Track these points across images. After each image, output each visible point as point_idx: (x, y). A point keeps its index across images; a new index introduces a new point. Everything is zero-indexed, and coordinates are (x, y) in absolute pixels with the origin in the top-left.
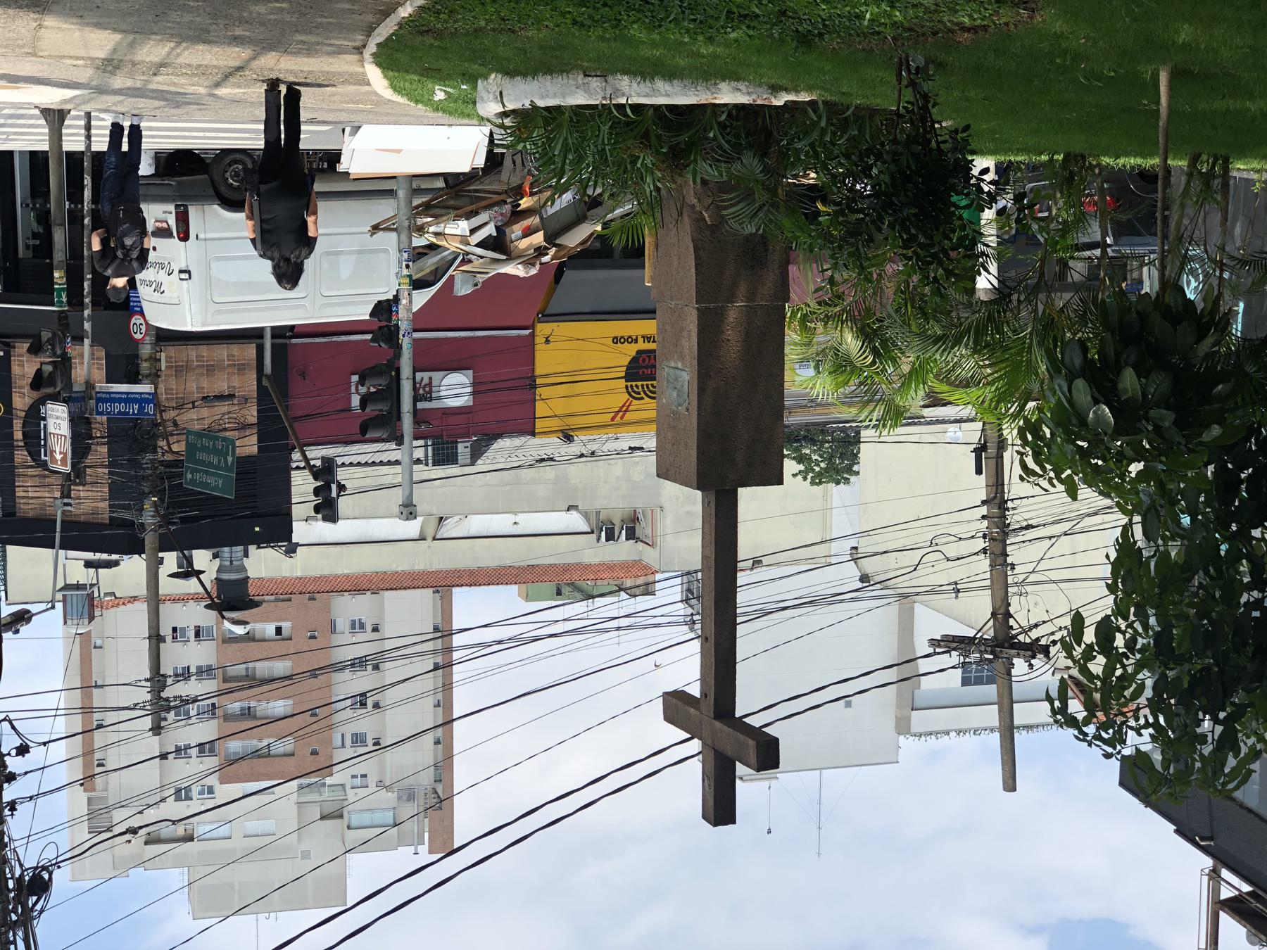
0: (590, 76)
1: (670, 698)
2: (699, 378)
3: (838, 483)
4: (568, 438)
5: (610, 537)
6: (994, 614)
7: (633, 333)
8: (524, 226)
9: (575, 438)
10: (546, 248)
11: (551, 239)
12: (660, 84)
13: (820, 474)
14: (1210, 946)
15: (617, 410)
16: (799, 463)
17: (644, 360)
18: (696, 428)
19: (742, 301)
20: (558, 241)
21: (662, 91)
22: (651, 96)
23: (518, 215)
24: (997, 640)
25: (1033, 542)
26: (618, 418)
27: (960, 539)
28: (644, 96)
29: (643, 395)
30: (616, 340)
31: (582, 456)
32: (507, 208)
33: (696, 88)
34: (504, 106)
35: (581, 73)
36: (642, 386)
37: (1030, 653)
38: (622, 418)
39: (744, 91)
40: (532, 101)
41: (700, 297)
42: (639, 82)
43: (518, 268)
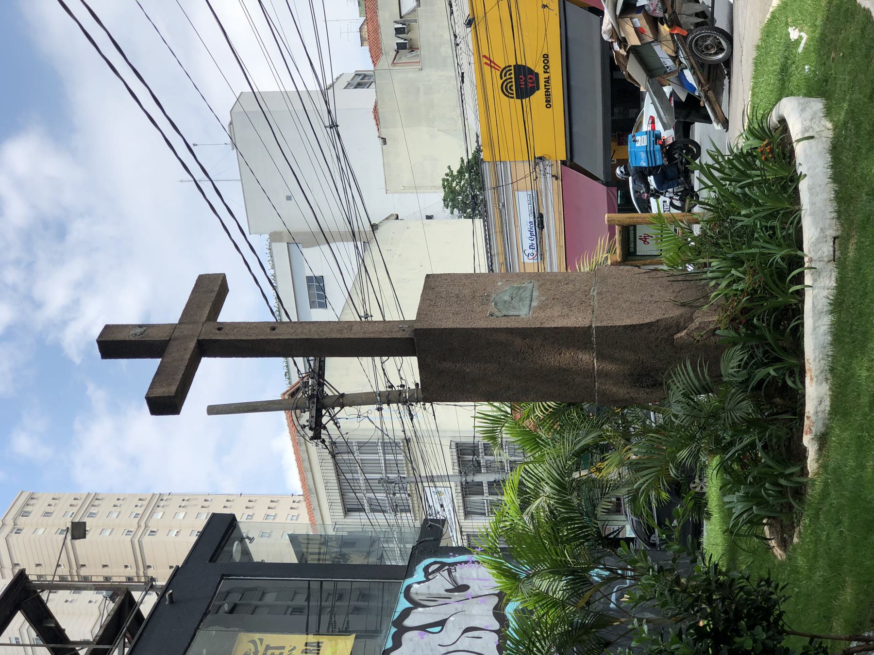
0: (834, 243)
1: (220, 282)
2: (523, 328)
3: (444, 200)
4: (470, 23)
5: (399, 31)
6: (342, 395)
7: (551, 70)
8: (644, 28)
9: (469, 29)
10: (625, 47)
11: (634, 50)
12: (826, 321)
13: (450, 187)
14: (94, 585)
15: (492, 59)
16: (459, 172)
17: (530, 79)
18: (474, 326)
19: (598, 367)
20: (631, 55)
21: (820, 323)
22: (813, 311)
23: (654, 22)
24: (322, 399)
25: (400, 419)
26: (485, 60)
27: (399, 370)
28: (813, 303)
29: (504, 78)
30: (546, 57)
31: (455, 36)
32: (659, 13)
33: (823, 359)
34: (798, 141)
35: (839, 233)
36: (511, 78)
37: (314, 426)
38: (486, 63)
39: (819, 409)
40: (805, 175)
41: (601, 330)
42: (828, 298)
43: (608, 24)
